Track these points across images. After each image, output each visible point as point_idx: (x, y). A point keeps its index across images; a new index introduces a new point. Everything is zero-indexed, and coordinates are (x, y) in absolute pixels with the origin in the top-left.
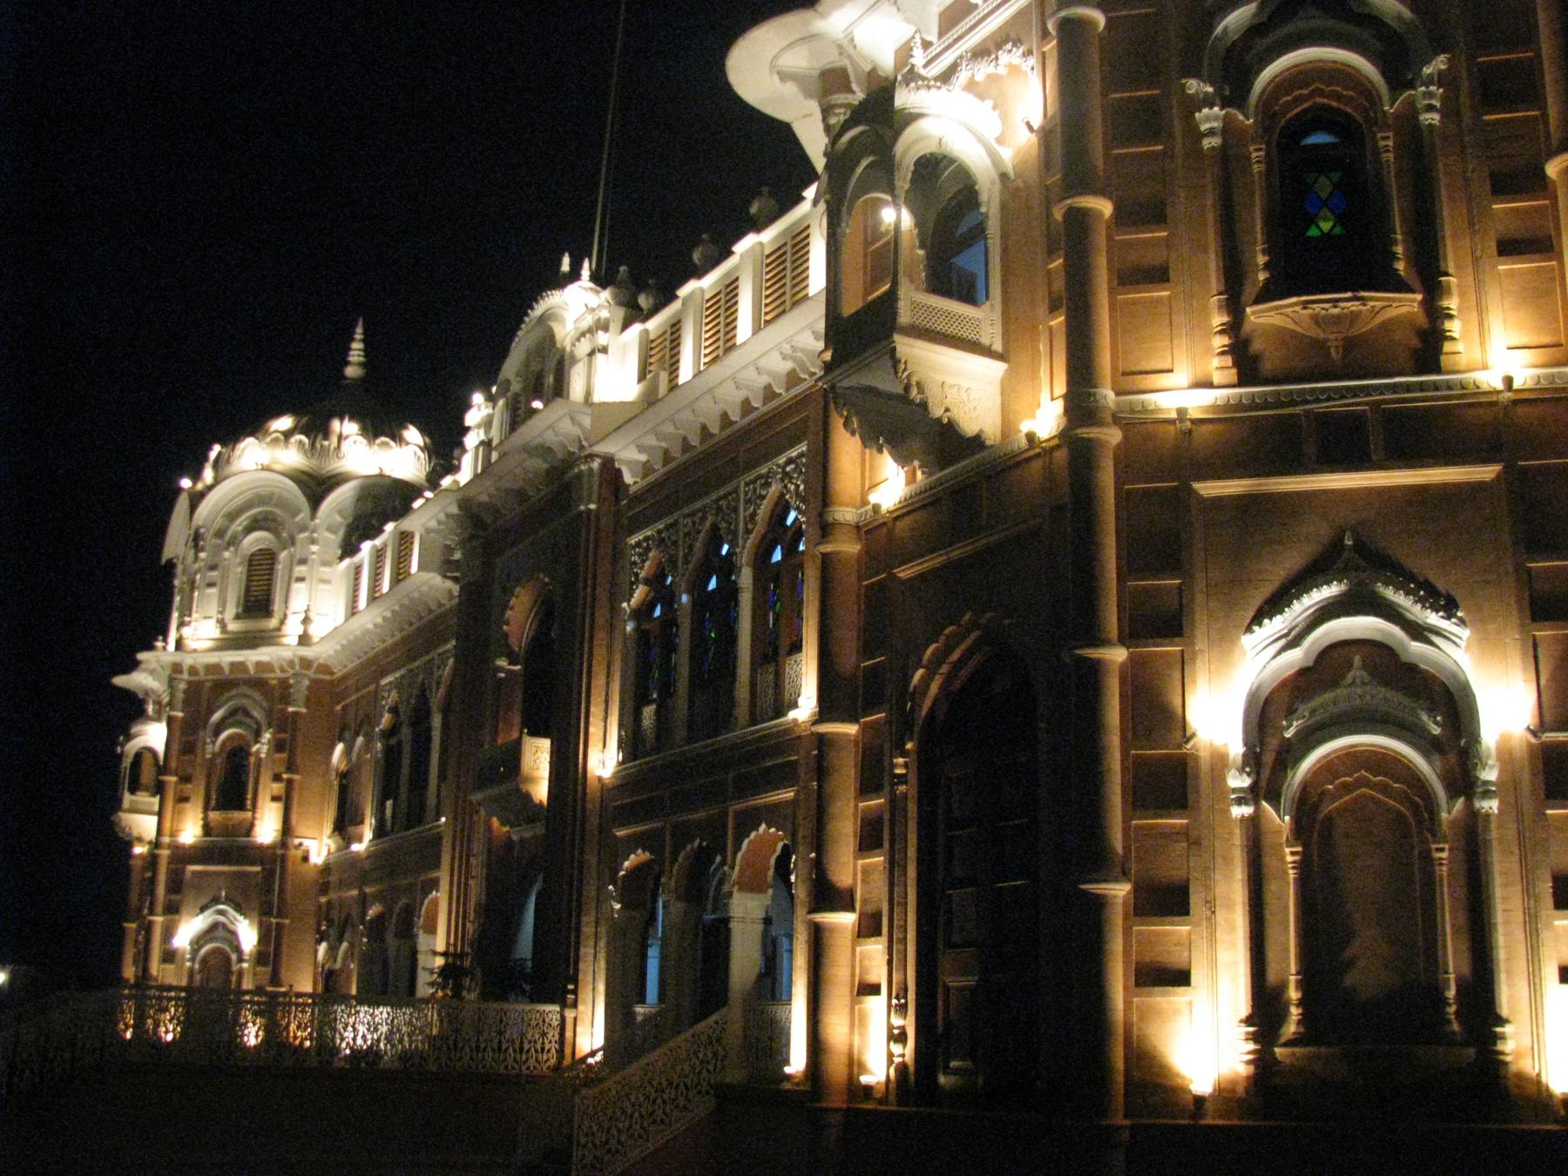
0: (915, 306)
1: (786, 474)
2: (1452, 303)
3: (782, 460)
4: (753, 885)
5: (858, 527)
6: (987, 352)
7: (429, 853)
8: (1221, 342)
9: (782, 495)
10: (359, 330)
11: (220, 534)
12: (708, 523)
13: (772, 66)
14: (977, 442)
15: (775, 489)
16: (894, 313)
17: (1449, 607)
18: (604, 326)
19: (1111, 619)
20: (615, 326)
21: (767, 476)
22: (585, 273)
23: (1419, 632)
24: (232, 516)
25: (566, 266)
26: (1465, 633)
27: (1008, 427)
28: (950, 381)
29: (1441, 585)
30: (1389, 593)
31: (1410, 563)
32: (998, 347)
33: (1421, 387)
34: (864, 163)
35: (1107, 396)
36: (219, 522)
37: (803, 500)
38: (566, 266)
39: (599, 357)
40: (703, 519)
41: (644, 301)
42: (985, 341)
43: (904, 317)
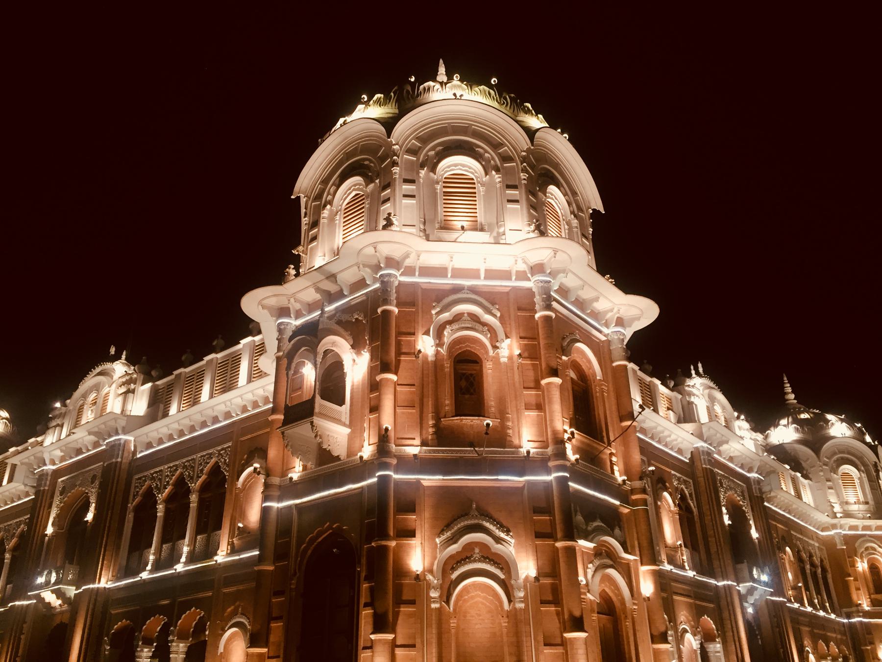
0: (321, 405)
1: (220, 454)
3: (219, 448)
4: (182, 637)
5: (280, 486)
6: (344, 425)
7: (825, 635)
8: (431, 430)
9: (217, 462)
12: (178, 472)
13: (260, 303)
14: (338, 458)
15: (213, 460)
16: (313, 408)
17: (508, 532)
18: (134, 381)
20: (139, 382)
21: (211, 454)
22: (124, 357)
23: (498, 540)
24: (425, 140)
25: (113, 351)
26: (513, 541)
27: (350, 453)
28: (331, 434)
29: (504, 524)
30: (487, 525)
31: (496, 515)
32: (348, 423)
33: (499, 452)
34: (303, 349)
35: (393, 447)
37: (228, 466)
38: (113, 351)
39: (131, 395)
40: (176, 470)
41: (153, 373)
42: (343, 420)
43: (317, 410)
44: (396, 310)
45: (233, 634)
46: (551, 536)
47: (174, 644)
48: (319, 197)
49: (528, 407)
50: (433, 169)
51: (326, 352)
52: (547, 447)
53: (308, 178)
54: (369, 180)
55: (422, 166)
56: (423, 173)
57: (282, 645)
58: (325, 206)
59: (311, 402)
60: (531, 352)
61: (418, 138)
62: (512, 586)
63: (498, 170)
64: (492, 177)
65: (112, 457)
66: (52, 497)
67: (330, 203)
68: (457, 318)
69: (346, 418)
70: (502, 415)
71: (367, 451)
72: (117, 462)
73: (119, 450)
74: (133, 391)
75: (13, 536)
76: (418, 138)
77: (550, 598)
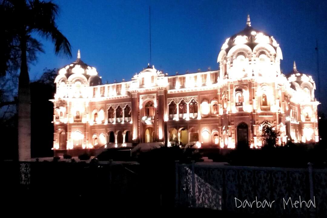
36: (71, 80)
59: (58, 117)
70: (81, 118)
75: (124, 106)
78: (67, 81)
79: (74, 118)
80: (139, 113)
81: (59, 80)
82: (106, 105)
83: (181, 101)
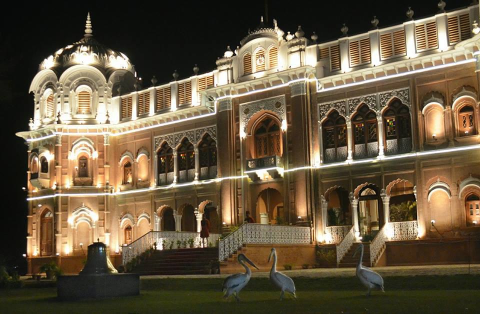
2: (94, 179)
10: (89, 17)
11: (68, 85)
19: (60, 210)
24: (72, 79)
36: (68, 81)
44: (61, 145)
45: (142, 220)
46: (104, 210)
47: (198, 215)
48: (39, 92)
49: (100, 174)
50: (75, 91)
51: (42, 157)
52: (104, 185)
53: (34, 86)
54: (55, 91)
55: (71, 90)
56: (71, 92)
57: (175, 221)
58: (41, 96)
60: (101, 156)
61: (69, 79)
62: (66, 226)
63: (97, 90)
64: (95, 93)
65: (300, 92)
66: (237, 113)
67: (42, 95)
68: (81, 146)
69: (48, 177)
70: (92, 177)
71: (54, 187)
72: (303, 96)
73: (303, 87)
74: (304, 50)
76: (69, 79)
77: (102, 225)
78: (58, 85)
79: (74, 177)
80: (239, 151)
81: (41, 86)
82: (151, 140)
83: (161, 143)
